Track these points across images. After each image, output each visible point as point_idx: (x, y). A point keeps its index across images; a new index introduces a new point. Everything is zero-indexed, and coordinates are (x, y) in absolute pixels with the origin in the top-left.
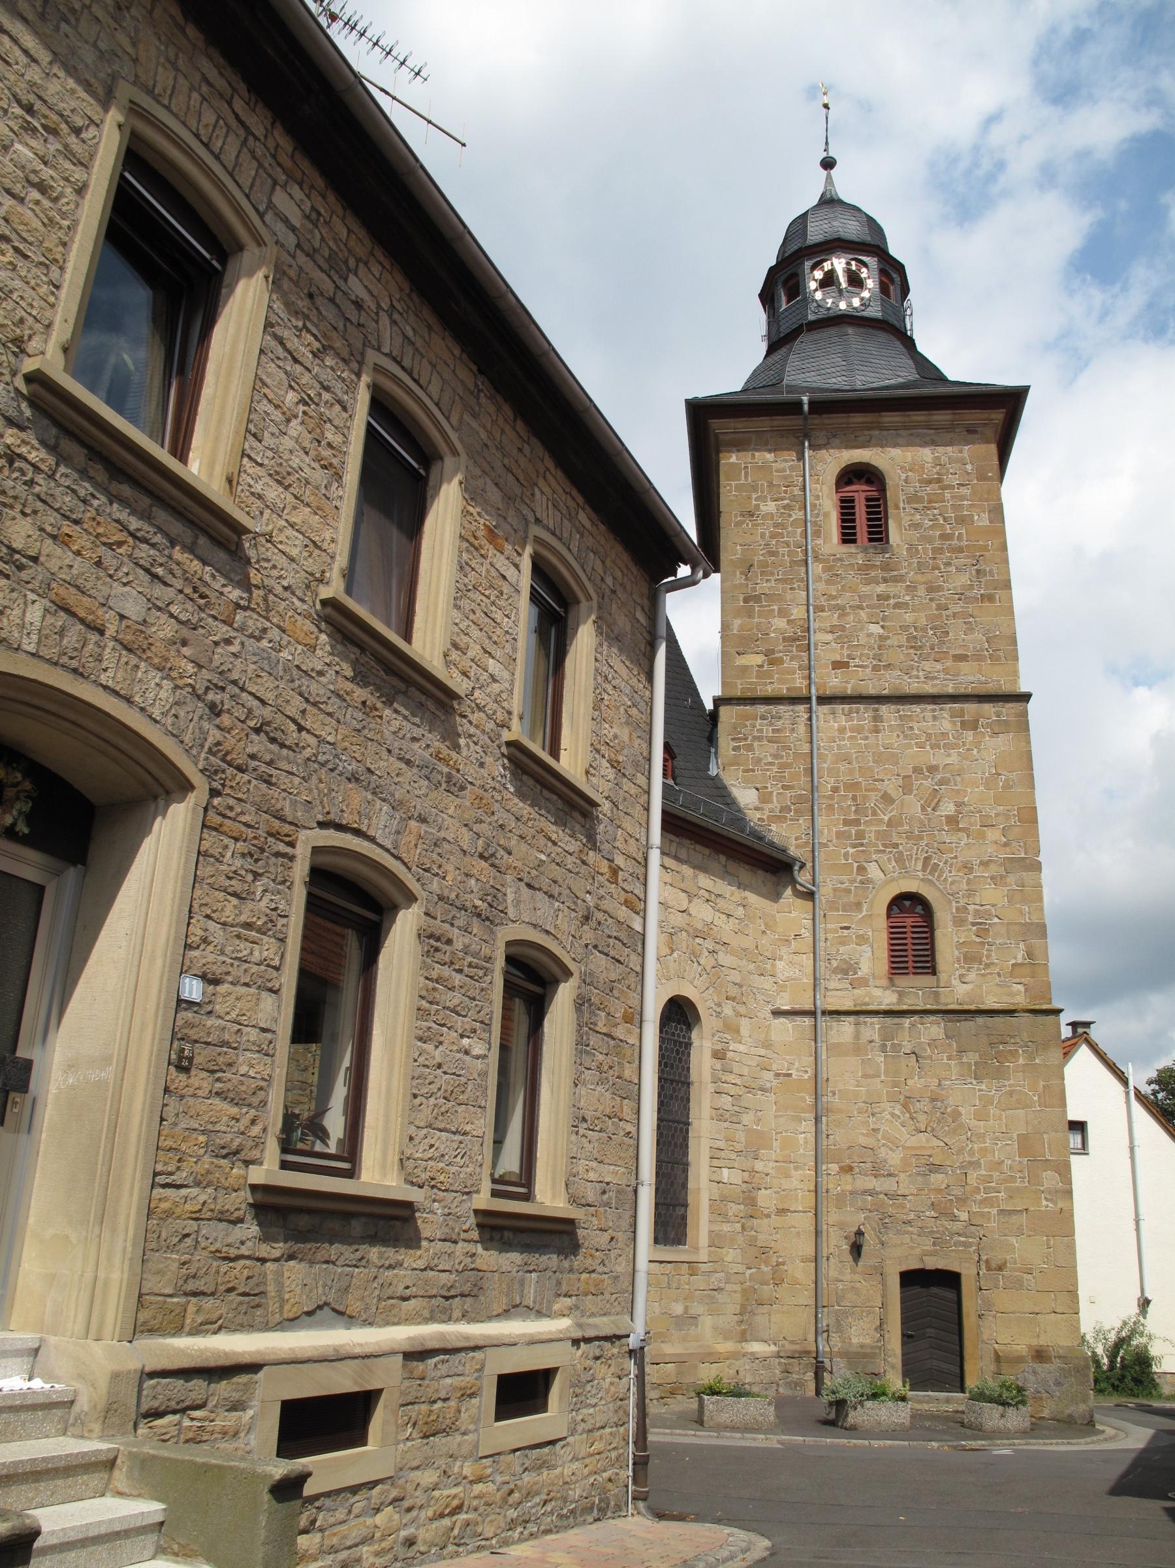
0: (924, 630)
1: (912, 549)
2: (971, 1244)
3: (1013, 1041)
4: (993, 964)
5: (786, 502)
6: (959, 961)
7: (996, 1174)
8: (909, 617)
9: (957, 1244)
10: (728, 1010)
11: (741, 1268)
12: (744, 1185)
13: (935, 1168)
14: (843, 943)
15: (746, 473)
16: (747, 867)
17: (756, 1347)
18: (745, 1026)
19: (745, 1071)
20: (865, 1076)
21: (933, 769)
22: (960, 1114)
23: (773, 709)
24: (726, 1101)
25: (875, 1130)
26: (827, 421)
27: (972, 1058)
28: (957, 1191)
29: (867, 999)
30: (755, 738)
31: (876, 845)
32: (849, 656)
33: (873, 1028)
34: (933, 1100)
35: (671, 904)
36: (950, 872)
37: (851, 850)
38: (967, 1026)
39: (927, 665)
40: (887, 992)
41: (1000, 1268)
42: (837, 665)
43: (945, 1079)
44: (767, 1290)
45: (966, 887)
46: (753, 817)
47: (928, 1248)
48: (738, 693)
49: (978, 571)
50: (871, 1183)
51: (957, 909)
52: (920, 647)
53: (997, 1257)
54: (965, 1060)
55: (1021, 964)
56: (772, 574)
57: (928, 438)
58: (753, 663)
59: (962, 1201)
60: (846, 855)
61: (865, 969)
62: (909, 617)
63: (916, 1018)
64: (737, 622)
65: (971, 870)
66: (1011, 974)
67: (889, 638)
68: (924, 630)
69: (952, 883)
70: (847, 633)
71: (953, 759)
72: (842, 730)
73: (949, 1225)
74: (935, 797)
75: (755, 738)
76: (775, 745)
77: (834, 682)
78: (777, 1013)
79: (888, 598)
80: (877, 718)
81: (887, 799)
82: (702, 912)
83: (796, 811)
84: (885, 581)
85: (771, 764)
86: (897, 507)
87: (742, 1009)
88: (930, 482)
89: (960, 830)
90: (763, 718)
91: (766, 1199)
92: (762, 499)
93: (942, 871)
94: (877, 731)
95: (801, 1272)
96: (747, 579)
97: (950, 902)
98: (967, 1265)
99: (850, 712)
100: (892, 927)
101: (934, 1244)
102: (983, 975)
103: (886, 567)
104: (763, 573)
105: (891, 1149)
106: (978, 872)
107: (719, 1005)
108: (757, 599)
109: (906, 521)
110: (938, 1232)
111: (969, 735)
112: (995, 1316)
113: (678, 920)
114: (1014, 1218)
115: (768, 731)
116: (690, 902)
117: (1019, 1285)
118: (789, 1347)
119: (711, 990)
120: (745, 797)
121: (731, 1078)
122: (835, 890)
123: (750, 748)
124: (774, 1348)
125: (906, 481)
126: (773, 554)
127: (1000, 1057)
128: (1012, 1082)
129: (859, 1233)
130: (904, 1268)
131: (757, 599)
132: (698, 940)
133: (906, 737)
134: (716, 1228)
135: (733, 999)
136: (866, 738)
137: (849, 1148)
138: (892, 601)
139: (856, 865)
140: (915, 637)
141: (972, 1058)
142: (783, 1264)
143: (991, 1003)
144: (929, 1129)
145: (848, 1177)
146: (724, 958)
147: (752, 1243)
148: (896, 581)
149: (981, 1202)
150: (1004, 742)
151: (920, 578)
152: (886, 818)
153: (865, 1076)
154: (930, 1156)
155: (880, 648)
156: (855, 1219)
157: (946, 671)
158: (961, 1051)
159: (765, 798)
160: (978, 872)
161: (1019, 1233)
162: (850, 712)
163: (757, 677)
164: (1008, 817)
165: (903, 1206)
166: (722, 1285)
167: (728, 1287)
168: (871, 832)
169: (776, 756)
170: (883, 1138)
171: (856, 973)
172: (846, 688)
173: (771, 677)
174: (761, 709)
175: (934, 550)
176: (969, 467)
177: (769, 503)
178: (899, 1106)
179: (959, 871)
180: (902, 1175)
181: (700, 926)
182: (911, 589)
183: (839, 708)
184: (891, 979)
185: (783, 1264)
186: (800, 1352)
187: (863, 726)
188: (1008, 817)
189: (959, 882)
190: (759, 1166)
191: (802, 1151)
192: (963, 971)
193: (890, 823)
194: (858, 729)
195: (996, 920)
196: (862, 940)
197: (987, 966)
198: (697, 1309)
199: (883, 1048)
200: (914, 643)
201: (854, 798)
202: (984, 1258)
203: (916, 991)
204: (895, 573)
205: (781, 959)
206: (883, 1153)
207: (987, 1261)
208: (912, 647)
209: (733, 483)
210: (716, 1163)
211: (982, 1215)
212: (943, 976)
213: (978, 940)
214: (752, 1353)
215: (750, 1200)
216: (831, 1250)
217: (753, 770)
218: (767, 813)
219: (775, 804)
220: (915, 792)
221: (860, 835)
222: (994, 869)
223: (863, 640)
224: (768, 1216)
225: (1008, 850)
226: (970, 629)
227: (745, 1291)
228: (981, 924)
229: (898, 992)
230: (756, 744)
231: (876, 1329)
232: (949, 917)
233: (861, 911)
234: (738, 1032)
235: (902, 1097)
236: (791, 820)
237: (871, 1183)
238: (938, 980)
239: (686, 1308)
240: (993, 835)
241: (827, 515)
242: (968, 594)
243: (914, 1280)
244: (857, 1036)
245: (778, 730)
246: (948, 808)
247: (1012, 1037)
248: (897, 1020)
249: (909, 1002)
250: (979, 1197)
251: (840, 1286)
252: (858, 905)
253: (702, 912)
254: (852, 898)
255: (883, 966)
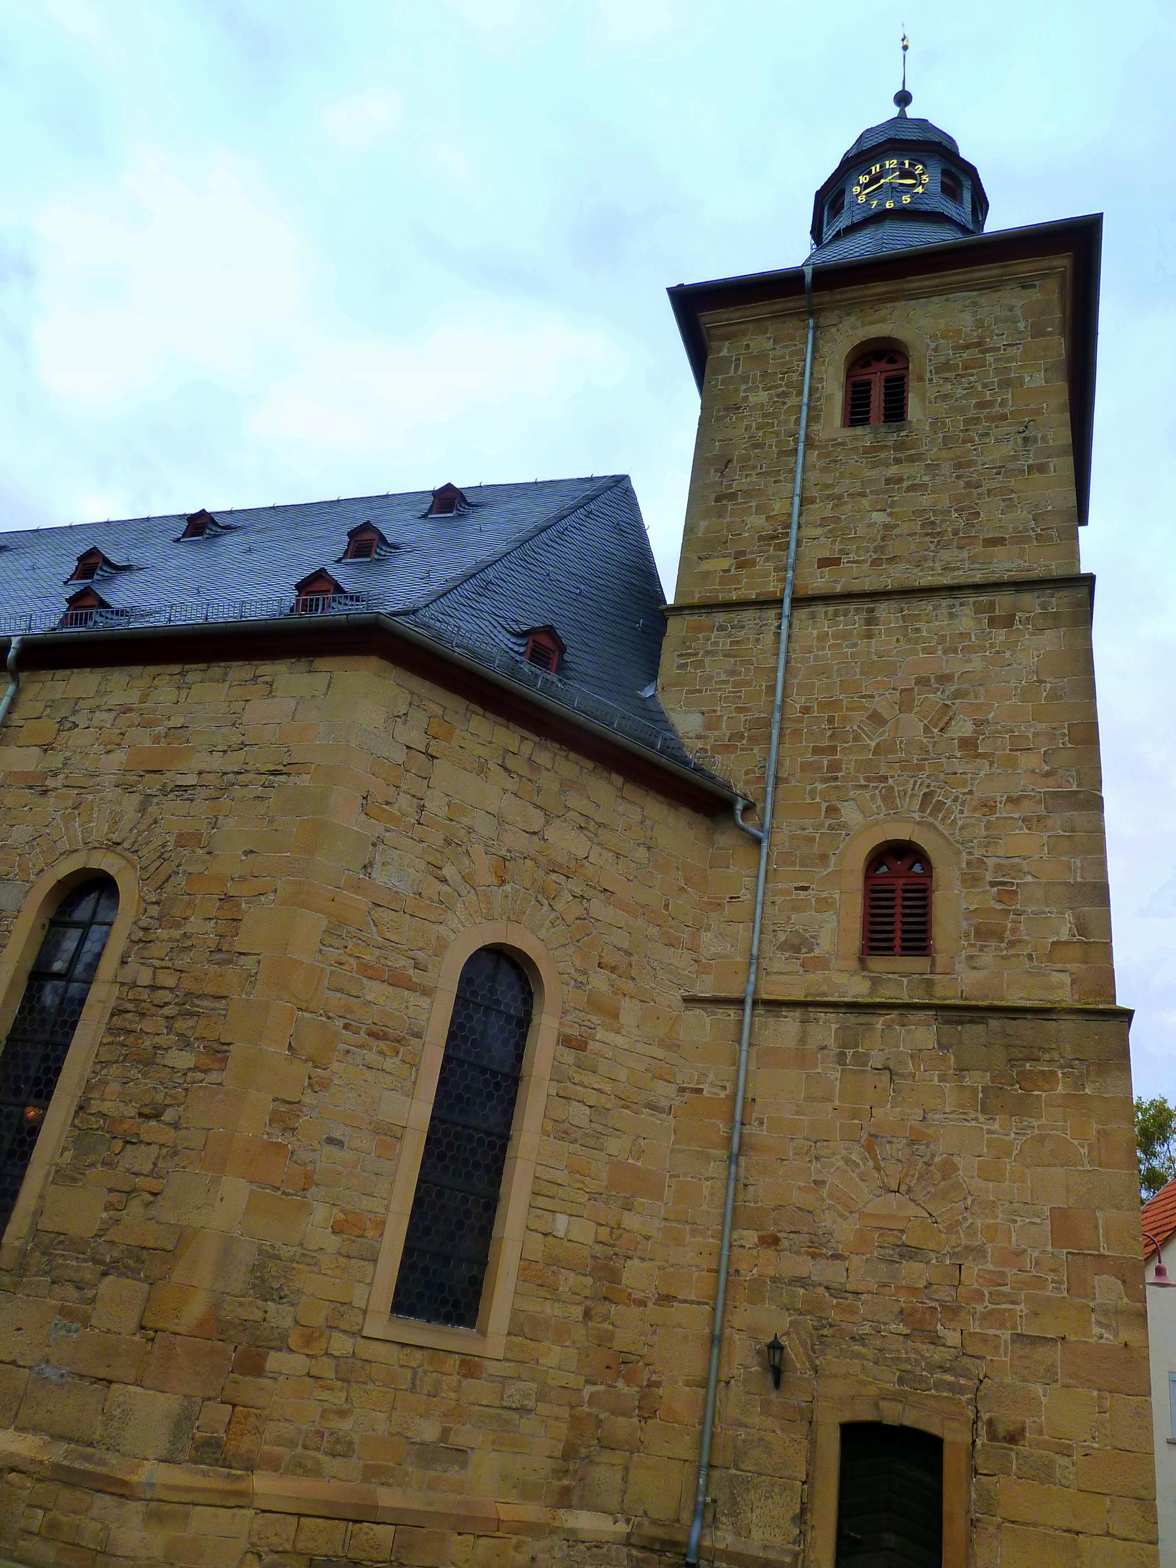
0: (947, 512)
1: (937, 423)
2: (961, 1390)
3: (1047, 1057)
4: (1020, 941)
5: (780, 390)
6: (967, 935)
7: (1011, 1273)
8: (925, 500)
9: (938, 1385)
10: (600, 982)
11: (575, 1381)
12: (598, 1247)
13: (910, 1252)
14: (796, 909)
15: (737, 366)
16: (661, 799)
17: (585, 1522)
18: (629, 1012)
19: (622, 1075)
20: (810, 1099)
21: (944, 679)
22: (955, 1168)
23: (736, 617)
24: (578, 1114)
25: (819, 1183)
26: (839, 297)
27: (978, 1080)
28: (945, 1294)
29: (824, 988)
30: (707, 653)
31: (856, 779)
32: (842, 551)
33: (826, 1029)
34: (913, 1142)
35: (510, 818)
36: (962, 812)
37: (820, 786)
38: (973, 1033)
39: (945, 555)
40: (856, 978)
41: (1013, 1438)
42: (824, 563)
43: (935, 1111)
44: (623, 1427)
45: (985, 833)
46: (692, 749)
47: (890, 1386)
48: (695, 601)
49: (1026, 440)
50: (806, 1267)
51: (969, 863)
52: (939, 533)
53: (1008, 1419)
54: (967, 1082)
55: (1066, 943)
56: (754, 468)
57: (967, 302)
58: (718, 568)
59: (952, 1311)
60: (813, 792)
61: (825, 945)
62: (925, 500)
63: (894, 1014)
64: (704, 524)
65: (992, 809)
66: (1050, 957)
67: (897, 526)
68: (947, 512)
69: (962, 828)
70: (843, 524)
71: (976, 663)
72: (823, 637)
73: (926, 1349)
74: (944, 714)
75: (707, 653)
76: (732, 660)
77: (819, 582)
78: (691, 1001)
79: (900, 480)
80: (870, 621)
81: (876, 719)
82: (566, 841)
83: (750, 739)
84: (898, 461)
85: (724, 682)
86: (921, 379)
87: (628, 986)
88: (967, 347)
89: (978, 756)
90: (721, 628)
91: (636, 1275)
92: (754, 389)
93: (949, 812)
94: (869, 635)
95: (678, 1395)
96: (722, 476)
97: (959, 852)
98: (954, 1425)
99: (836, 614)
100: (874, 892)
101: (901, 1381)
102: (1003, 957)
103: (900, 446)
104: (742, 468)
105: (841, 1215)
106: (1003, 811)
107: (585, 973)
108: (732, 496)
109: (932, 393)
110: (908, 1360)
111: (1000, 635)
112: (999, 1527)
113: (518, 842)
114: (1041, 1352)
115: (725, 644)
116: (547, 822)
117: (1045, 1474)
118: (650, 1530)
119: (571, 949)
120: (686, 723)
121: (588, 1079)
122: (792, 838)
123: (699, 664)
124: (622, 1528)
125: (936, 350)
126: (756, 446)
127: (1025, 1079)
128: (1044, 1121)
129: (775, 1346)
130: (847, 1417)
131: (732, 496)
132: (554, 876)
133: (909, 641)
134: (531, 1306)
135: (613, 969)
136: (855, 645)
137: (778, 1207)
138: (905, 484)
139: (824, 805)
140: (933, 523)
141: (978, 1080)
142: (658, 1384)
143: (1015, 998)
144: (903, 1188)
145: (770, 1253)
146: (597, 907)
147: (604, 1340)
148: (913, 461)
149: (985, 1317)
150: (1051, 640)
151: (945, 454)
152: (873, 744)
153: (810, 1099)
154: (902, 1231)
155: (883, 539)
156: (771, 1320)
157: (973, 559)
158: (961, 1070)
159: (711, 724)
160: (1003, 811)
161: (1049, 1376)
162: (836, 614)
163: (720, 584)
164: (1053, 737)
165: (853, 1311)
166: (530, 1404)
167: (542, 1408)
168: (849, 763)
169: (732, 673)
170: (830, 1196)
171: (811, 950)
172: (834, 588)
173: (738, 582)
174: (720, 618)
175: (968, 422)
176: (1021, 325)
177: (761, 393)
178: (858, 1148)
179: (974, 810)
180: (856, 1259)
181: (562, 859)
182: (932, 468)
183: (820, 609)
184: (861, 961)
185: (658, 1384)
186: (663, 1542)
187: (851, 632)
188: (1053, 737)
189: (973, 825)
190: (631, 1221)
191: (705, 1207)
192: (974, 952)
193: (877, 751)
194: (845, 635)
195: (1029, 879)
196: (824, 904)
197: (1012, 944)
198: (464, 1435)
199: (841, 1058)
200: (931, 530)
201: (831, 720)
202: (985, 1416)
203: (899, 976)
204: (913, 452)
205: (708, 929)
206: (827, 1221)
207: (990, 1423)
208: (927, 534)
209: (720, 377)
210: (541, 1202)
211: (985, 1339)
212: (941, 959)
213: (998, 907)
214: (572, 1531)
215: (606, 1271)
216: (735, 1372)
217: (700, 691)
218: (711, 741)
219: (724, 731)
220: (916, 709)
221: (835, 767)
222: (1027, 808)
223: (861, 530)
224: (642, 1303)
225: (1051, 781)
226: (1010, 506)
227: (576, 1421)
228: (1005, 883)
229: (871, 978)
230: (707, 660)
231: (793, 1519)
232: (957, 874)
233: (827, 866)
234: (616, 1016)
235: (864, 1136)
236: (742, 749)
237: (806, 1267)
238: (933, 964)
239: (446, 1432)
240: (1030, 761)
241: (830, 397)
242: (1010, 466)
243: (861, 1439)
244: (803, 1040)
245: (738, 642)
246: (964, 727)
247: (1045, 1050)
248: (864, 1019)
249: (887, 993)
250: (980, 1308)
251: (742, 1434)
252: (824, 858)
253: (566, 841)
254: (816, 849)
255: (855, 940)
